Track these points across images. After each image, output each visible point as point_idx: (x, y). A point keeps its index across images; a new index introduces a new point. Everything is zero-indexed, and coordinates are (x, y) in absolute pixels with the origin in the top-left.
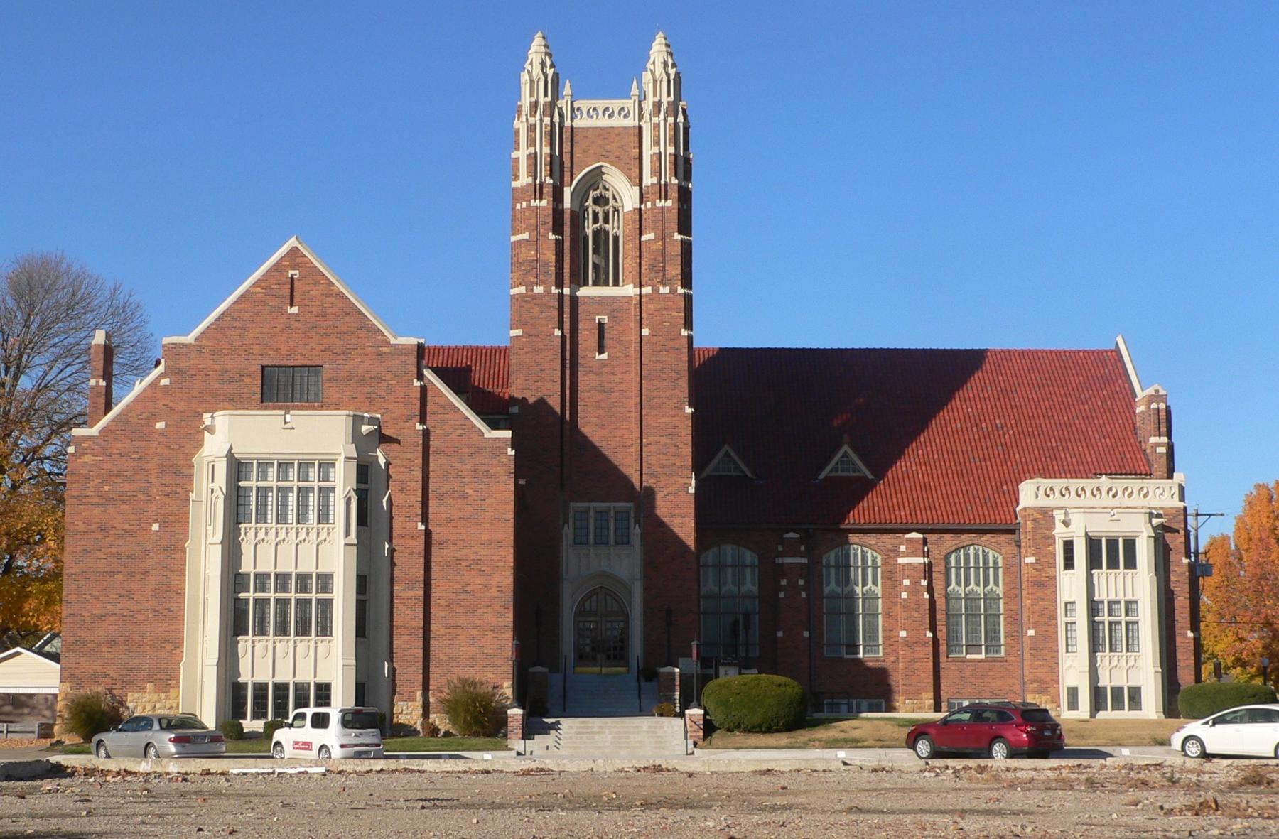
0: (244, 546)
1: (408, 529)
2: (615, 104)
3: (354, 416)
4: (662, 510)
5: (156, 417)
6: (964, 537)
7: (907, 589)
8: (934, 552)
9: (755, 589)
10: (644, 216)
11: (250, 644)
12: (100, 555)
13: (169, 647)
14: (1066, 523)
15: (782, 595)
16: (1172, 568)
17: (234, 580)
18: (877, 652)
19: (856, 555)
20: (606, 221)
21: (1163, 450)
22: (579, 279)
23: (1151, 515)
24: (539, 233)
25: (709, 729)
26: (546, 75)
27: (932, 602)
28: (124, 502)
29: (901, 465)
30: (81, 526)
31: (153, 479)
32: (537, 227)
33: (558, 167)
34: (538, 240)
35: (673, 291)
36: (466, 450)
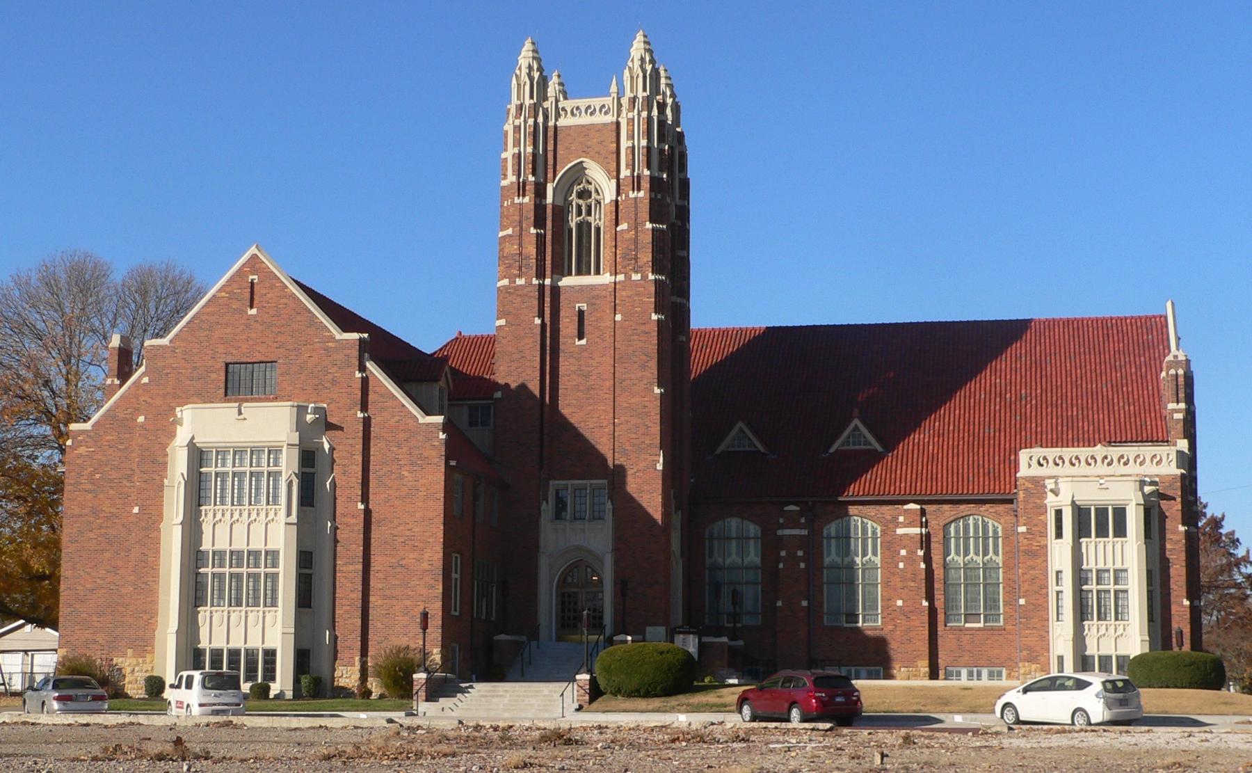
0: (204, 526)
1: (350, 508)
2: (596, 102)
3: (298, 407)
4: (632, 486)
5: (137, 411)
6: (962, 507)
7: (903, 559)
8: (932, 523)
9: (758, 560)
10: (621, 207)
11: (208, 614)
12: (92, 535)
13: (146, 617)
14: (1055, 492)
15: (781, 566)
16: (1168, 536)
17: (194, 556)
18: (998, 620)
19: (856, 526)
20: (589, 214)
21: (1180, 416)
22: (561, 269)
23: (1142, 483)
24: (521, 228)
25: (595, 692)
26: (531, 78)
27: (929, 572)
28: (111, 488)
29: (915, 437)
30: (77, 511)
31: (135, 467)
32: (521, 222)
33: (541, 164)
34: (521, 235)
35: (644, 278)
36: (402, 436)
